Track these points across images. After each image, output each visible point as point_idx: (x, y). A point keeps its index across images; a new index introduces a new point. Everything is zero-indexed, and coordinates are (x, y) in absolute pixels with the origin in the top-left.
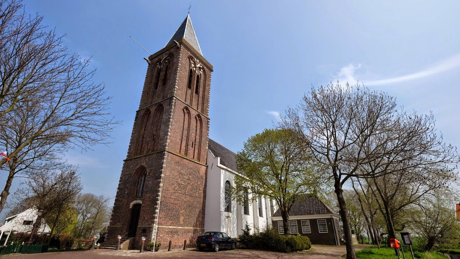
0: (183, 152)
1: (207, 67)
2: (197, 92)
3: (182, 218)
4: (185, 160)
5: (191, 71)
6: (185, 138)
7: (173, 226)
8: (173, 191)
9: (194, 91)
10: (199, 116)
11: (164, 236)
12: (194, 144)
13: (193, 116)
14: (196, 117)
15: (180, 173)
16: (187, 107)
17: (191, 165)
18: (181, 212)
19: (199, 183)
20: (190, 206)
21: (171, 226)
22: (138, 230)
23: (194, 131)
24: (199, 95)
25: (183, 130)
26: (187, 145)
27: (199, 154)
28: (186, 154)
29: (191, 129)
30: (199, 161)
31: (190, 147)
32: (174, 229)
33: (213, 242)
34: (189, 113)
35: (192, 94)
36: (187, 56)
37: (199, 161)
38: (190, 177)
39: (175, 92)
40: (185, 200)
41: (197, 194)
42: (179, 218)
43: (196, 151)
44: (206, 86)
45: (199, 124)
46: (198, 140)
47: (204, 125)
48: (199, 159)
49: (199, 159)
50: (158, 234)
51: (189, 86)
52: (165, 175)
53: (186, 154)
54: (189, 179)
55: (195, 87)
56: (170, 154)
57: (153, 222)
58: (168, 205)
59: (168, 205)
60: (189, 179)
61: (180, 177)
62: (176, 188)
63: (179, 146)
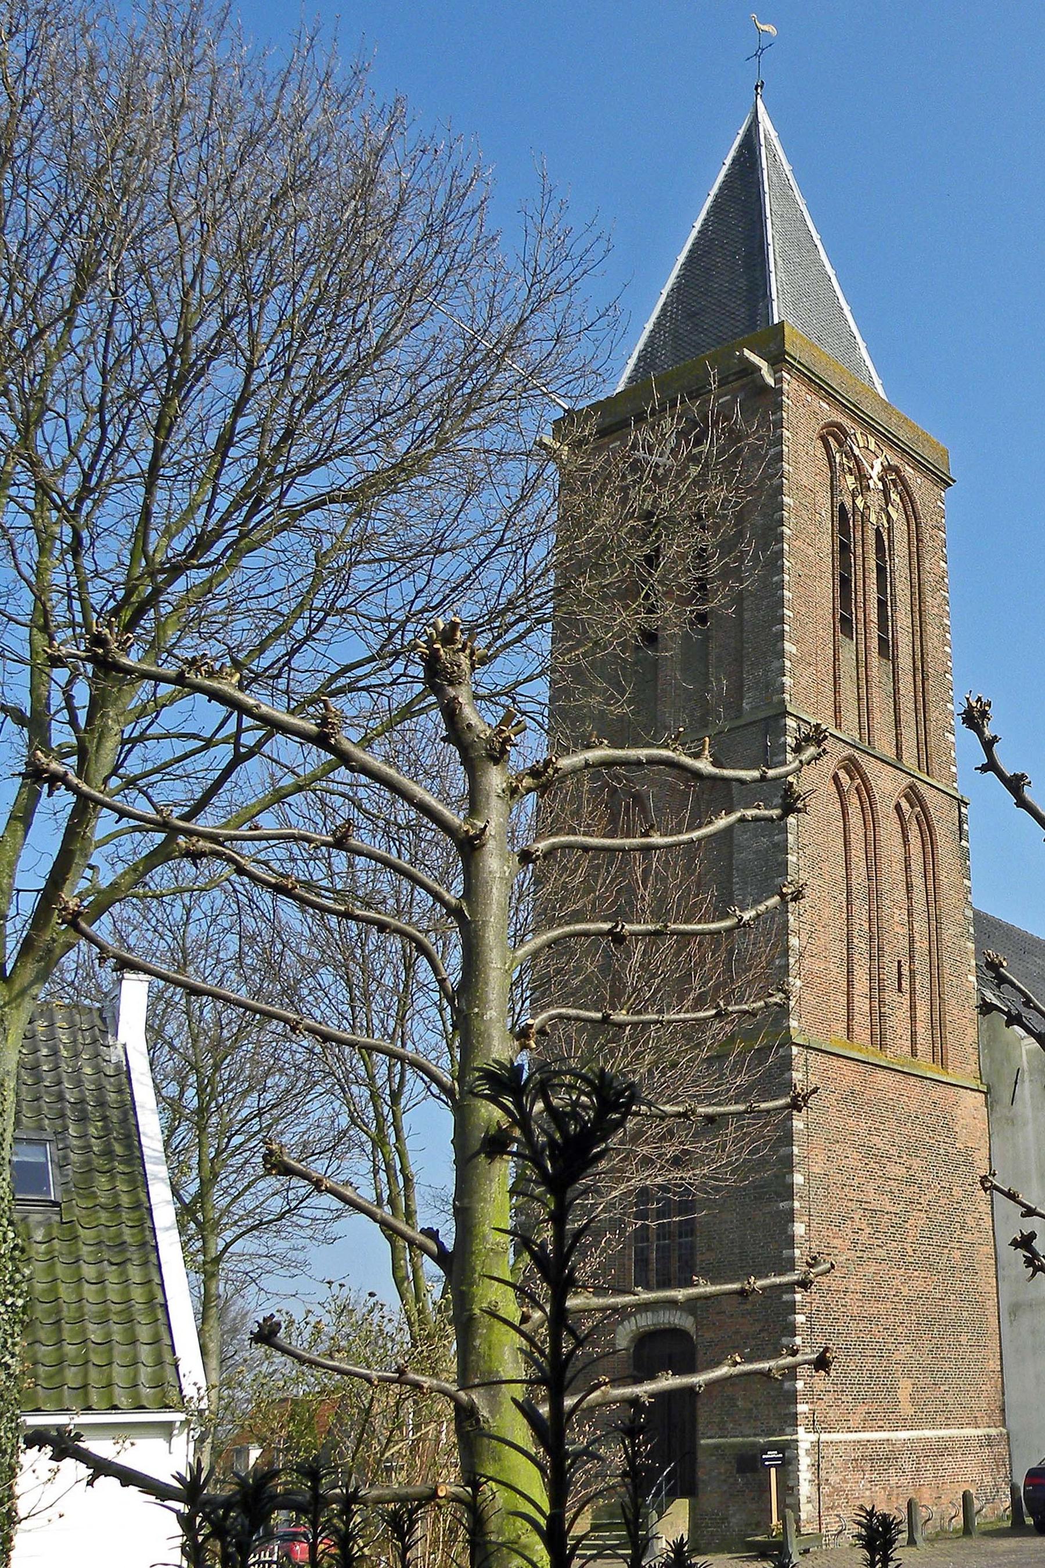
0: (862, 1034)
1: (920, 465)
2: (886, 648)
3: (905, 1388)
4: (881, 1075)
5: (842, 517)
6: (861, 945)
7: (872, 1429)
8: (851, 1254)
9: (874, 643)
10: (913, 795)
11: (845, 1481)
12: (905, 971)
13: (885, 810)
14: (836, 778)
15: (869, 1153)
16: (851, 759)
17: (913, 1097)
18: (897, 1356)
19: (957, 1192)
20: (931, 1323)
21: (864, 1429)
22: (701, 1458)
23: (901, 894)
24: (894, 661)
25: (849, 903)
26: (877, 986)
27: (938, 1024)
28: (879, 1039)
29: (886, 887)
30: (944, 1065)
31: (890, 996)
32: (882, 1442)
33: (543, 1310)
34: (865, 789)
35: (862, 664)
36: (816, 427)
37: (944, 1065)
38: (916, 1163)
39: (787, 680)
40: (905, 1291)
41: (957, 1254)
42: (892, 1389)
43: (922, 1012)
44: (927, 588)
45: (855, 820)
46: (921, 946)
47: (945, 845)
48: (940, 1058)
49: (940, 1058)
50: (823, 1473)
51: (845, 625)
52: (807, 1178)
53: (879, 1039)
54: (911, 1180)
55: (874, 617)
56: (812, 1056)
57: (792, 1420)
58: (840, 1327)
59: (840, 1327)
60: (911, 1180)
61: (871, 1176)
62: (863, 1237)
63: (843, 1000)
